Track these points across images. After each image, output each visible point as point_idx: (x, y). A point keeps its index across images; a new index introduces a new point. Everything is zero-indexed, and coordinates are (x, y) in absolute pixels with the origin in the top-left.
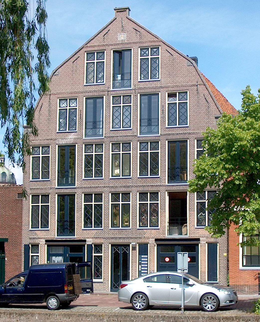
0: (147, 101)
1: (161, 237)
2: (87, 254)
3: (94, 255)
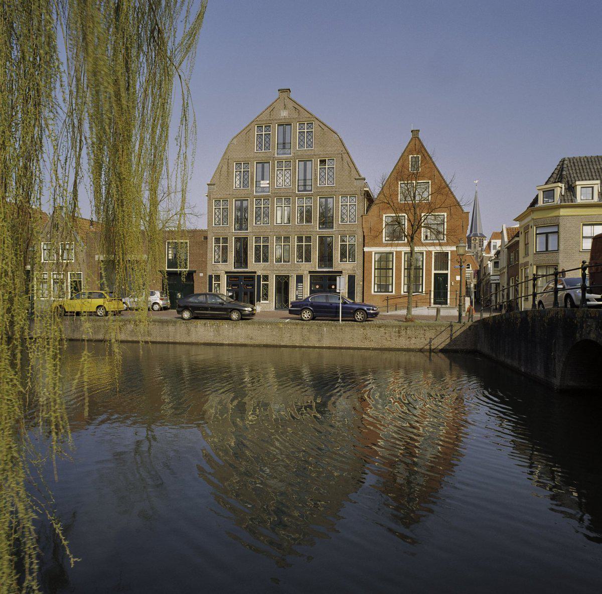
0: (303, 166)
1: (313, 270)
2: (372, 258)
3: (262, 283)
